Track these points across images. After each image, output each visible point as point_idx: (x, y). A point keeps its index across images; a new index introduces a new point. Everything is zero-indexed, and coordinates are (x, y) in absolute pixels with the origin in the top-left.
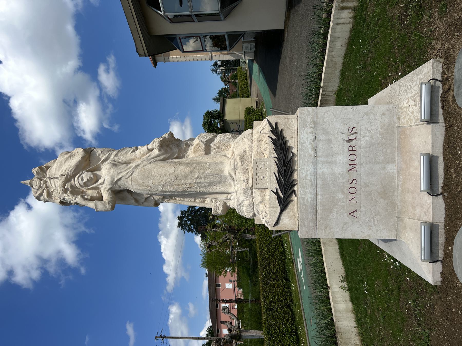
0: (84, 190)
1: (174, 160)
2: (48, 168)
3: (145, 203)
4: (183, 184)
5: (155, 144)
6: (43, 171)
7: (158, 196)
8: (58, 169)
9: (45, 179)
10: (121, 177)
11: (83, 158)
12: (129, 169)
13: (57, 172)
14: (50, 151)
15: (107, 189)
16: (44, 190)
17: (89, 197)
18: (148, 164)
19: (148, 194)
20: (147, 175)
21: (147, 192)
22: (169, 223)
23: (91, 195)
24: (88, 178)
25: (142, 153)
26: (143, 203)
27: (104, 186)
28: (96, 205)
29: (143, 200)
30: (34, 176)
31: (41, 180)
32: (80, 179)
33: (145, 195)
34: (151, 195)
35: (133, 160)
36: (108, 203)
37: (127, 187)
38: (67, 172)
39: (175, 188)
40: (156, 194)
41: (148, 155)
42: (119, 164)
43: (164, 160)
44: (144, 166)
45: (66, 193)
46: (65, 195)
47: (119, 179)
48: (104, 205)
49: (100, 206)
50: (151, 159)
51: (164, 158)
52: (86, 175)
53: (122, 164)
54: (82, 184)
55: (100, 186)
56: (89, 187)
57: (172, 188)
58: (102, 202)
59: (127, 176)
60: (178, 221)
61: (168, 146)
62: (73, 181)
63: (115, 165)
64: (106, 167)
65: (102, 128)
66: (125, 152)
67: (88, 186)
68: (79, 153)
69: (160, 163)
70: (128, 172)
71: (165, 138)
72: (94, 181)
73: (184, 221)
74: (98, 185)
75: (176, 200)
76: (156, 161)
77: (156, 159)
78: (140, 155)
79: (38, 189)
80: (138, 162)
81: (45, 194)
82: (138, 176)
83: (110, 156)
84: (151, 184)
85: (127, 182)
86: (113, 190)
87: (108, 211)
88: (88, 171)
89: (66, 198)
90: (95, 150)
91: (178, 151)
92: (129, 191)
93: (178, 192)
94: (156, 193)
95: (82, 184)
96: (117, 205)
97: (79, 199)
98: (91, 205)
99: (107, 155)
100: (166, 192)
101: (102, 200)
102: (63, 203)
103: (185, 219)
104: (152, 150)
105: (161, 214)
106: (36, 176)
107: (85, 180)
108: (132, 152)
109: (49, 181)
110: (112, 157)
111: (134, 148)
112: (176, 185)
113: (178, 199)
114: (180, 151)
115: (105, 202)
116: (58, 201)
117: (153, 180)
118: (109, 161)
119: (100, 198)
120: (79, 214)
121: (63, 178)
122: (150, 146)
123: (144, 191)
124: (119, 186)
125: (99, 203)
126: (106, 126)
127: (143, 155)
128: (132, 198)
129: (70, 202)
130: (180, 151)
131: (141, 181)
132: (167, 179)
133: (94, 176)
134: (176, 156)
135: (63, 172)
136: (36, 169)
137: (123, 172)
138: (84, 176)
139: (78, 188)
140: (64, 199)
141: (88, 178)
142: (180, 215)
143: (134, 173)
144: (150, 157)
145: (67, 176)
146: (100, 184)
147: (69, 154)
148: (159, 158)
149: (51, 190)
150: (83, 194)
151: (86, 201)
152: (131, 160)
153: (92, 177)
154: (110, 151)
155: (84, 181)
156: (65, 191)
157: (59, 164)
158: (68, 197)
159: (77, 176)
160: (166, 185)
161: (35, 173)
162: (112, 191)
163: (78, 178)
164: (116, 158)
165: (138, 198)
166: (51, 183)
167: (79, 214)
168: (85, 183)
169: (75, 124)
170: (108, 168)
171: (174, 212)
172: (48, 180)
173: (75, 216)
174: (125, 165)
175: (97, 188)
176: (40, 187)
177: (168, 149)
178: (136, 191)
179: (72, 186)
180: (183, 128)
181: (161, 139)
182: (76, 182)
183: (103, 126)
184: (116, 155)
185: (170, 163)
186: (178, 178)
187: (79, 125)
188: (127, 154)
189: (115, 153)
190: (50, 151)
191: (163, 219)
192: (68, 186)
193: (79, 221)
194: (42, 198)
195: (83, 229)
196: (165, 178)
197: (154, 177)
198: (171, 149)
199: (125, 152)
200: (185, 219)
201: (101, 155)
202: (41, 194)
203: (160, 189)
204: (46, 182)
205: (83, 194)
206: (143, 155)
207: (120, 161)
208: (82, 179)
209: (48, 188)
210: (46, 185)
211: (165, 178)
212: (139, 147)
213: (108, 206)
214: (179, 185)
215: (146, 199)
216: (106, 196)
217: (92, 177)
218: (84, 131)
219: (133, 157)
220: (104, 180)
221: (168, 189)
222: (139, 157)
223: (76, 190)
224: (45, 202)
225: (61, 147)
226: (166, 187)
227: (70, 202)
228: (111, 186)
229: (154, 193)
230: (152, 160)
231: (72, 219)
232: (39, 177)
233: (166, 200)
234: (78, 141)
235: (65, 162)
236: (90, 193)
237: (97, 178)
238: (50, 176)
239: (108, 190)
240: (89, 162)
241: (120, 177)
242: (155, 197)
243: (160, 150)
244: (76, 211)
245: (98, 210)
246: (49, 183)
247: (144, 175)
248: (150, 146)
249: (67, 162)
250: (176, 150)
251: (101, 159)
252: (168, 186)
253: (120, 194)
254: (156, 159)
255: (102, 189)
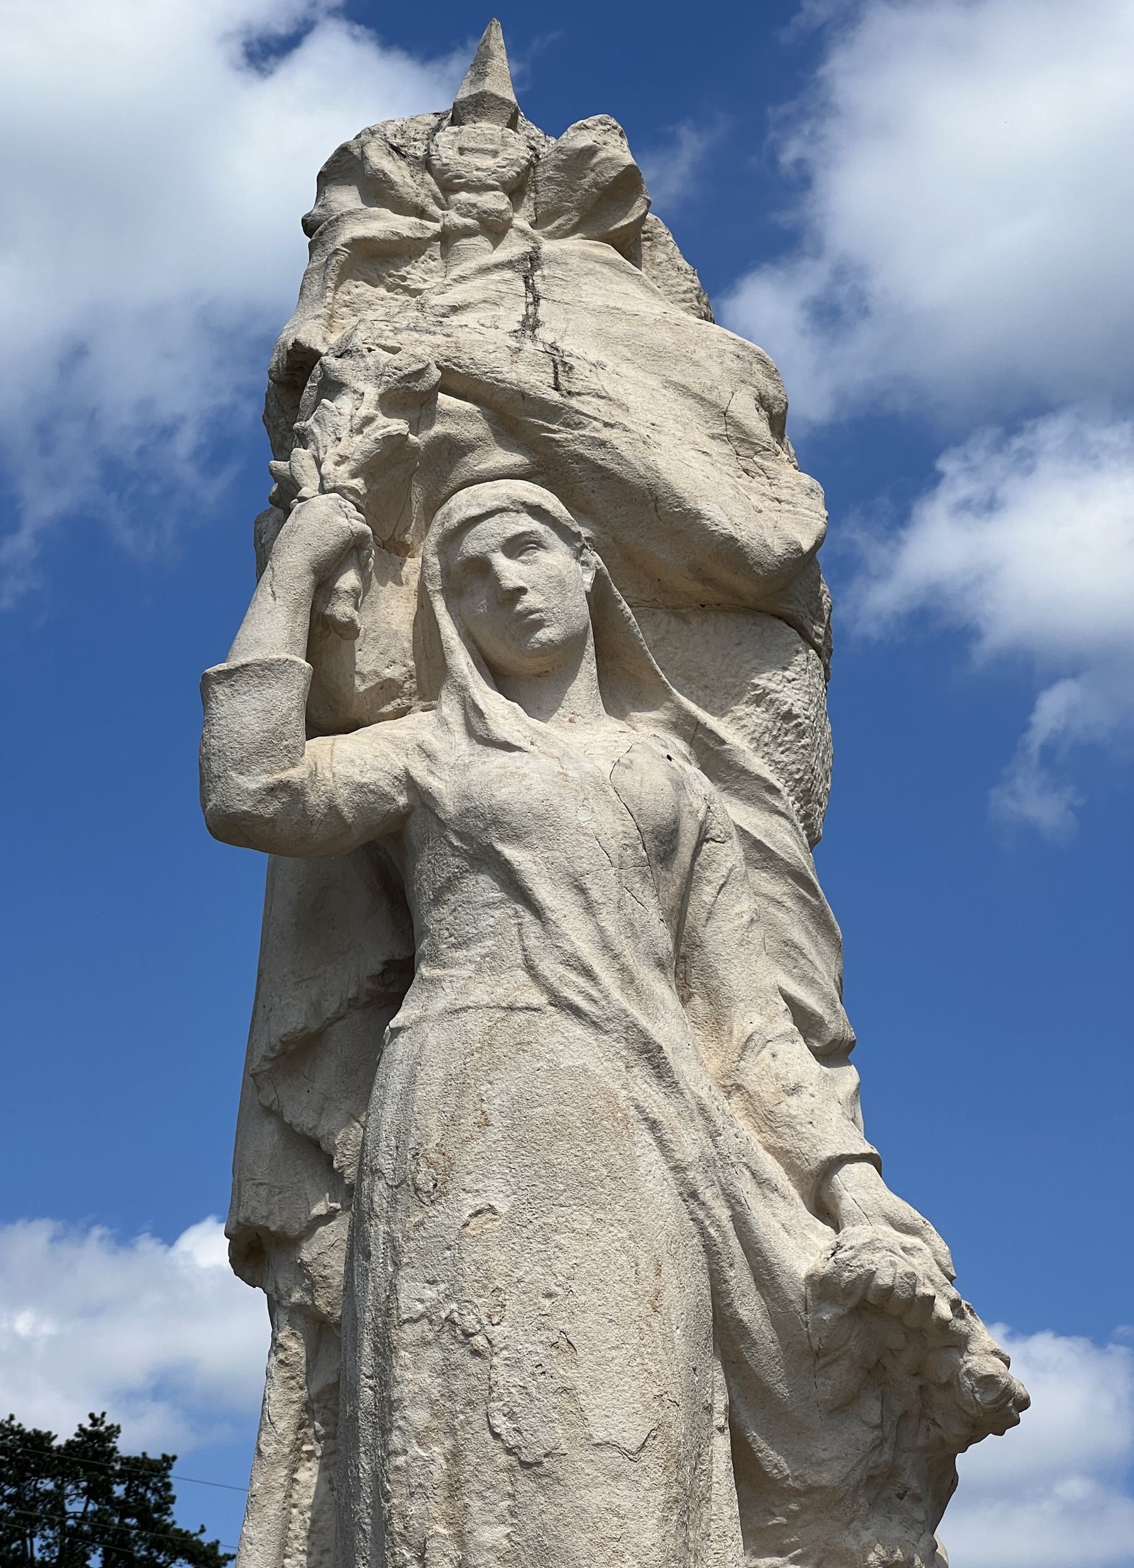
0: (411, 567)
1: (722, 1445)
2: (629, 245)
3: (267, 1136)
4: (461, 1538)
5: (890, 1239)
6: (602, 209)
7: (335, 1265)
8: (619, 328)
9: (521, 221)
10: (537, 911)
11: (730, 550)
12: (628, 978)
13: (591, 322)
14: (784, 218)
15: (420, 771)
16: (421, 212)
17: (342, 609)
18: (678, 1168)
19: (367, 1168)
20: (564, 1156)
21: (385, 1163)
22: (47, 1328)
23: (363, 621)
24: (530, 600)
25: (793, 1105)
26: (272, 1112)
27: (456, 744)
28: (267, 669)
29: (300, 1115)
30: (554, 129)
31: (516, 190)
32: (526, 523)
33: (355, 1133)
34: (350, 1195)
35: (717, 1022)
36: (285, 786)
37: (435, 959)
38: (587, 405)
39: (419, 1456)
40: (358, 1246)
41: (772, 1168)
42: (675, 880)
43: (725, 1335)
44: (654, 1126)
45: (390, 403)
46: (372, 392)
47: (515, 888)
48: (270, 747)
49: (253, 713)
50: (732, 1201)
51: (742, 1330)
52: (561, 584)
53: (678, 918)
54: (472, 545)
55: (450, 708)
56: (439, 605)
57: (419, 1416)
58: (298, 723)
59: (549, 967)
60: (64, 1433)
61: (874, 1373)
62: (503, 458)
63: (665, 848)
64: (640, 759)
65: (1024, 674)
66: (798, 935)
67: (454, 592)
68: (773, 511)
69: (683, 1291)
70: (587, 973)
71: (961, 1343)
72: (501, 652)
73: (56, 1499)
74: (462, 689)
75: (297, 1457)
76: (710, 1250)
77: (729, 1250)
78: (766, 1090)
79: (426, 164)
80: (696, 1070)
81: (384, 223)
82: (554, 1070)
83: (751, 799)
84: (472, 1202)
85: (492, 964)
86: (416, 827)
87: (205, 781)
88: (599, 598)
89: (344, 403)
90: (805, 661)
91: (825, 1478)
92: (396, 979)
93: (378, 1478)
94: (378, 1250)
95: (472, 545)
96: (259, 860)
97: (324, 518)
98: (271, 629)
99: (758, 765)
100: (385, 1350)
101: (315, 728)
102: (298, 377)
103: (76, 1506)
104: (825, 1209)
105: (147, 1245)
106: (548, 147)
107: (511, 572)
108: (796, 1008)
109: (502, 254)
110: (738, 813)
111: (838, 1024)
112: (455, 1456)
113: (309, 1474)
114: (822, 1501)
115: (293, 755)
116: (311, 333)
117: (515, 1224)
118: (701, 784)
119: (331, 710)
120: (188, 473)
121: (532, 376)
122: (859, 1186)
123: (402, 1133)
124: (450, 885)
125: (286, 698)
126: (1053, 708)
127: (767, 1120)
128: (331, 1006)
129: (303, 439)
130: (822, 1501)
131: (498, 1093)
132: (515, 1364)
133: (550, 647)
134: (772, 1458)
135: (583, 377)
136: (618, 151)
137: (597, 926)
138: (557, 558)
139: (432, 507)
140: (333, 387)
141: (530, 600)
142: (127, 1445)
143: (577, 1030)
144: (745, 1186)
145: (553, 412)
146: (473, 713)
147: (759, 426)
148: (739, 1277)
149: (415, 274)
150: (372, 550)
151: (305, 584)
152: (713, 996)
153: (544, 635)
154: (806, 797)
155: (501, 563)
156: (408, 396)
157: (664, 337)
158: (346, 428)
159: (551, 502)
160: (459, 1354)
161: (578, 138)
162: (403, 817)
163: (537, 512)
164: (728, 856)
165: (326, 1072)
166: (485, 270)
167: (188, 473)
168: (482, 567)
169: (1051, 433)
170: (627, 779)
171: (165, 1387)
172: (513, 248)
173: (167, 432)
174: (665, 942)
175: (430, 677)
176: (449, 184)
177: (838, 1378)
178: (399, 1050)
179: (452, 450)
180: (1075, 1488)
181: (943, 1309)
182: (496, 496)
183: (1052, 679)
184: (760, 854)
185: (693, 1392)
186: (526, 1485)
187: (1046, 467)
188: (768, 954)
189: (786, 840)
190: (784, 218)
191: (94, 1265)
192: (457, 417)
193: (114, 474)
194: (346, 198)
195: (43, 505)
196: (533, 1347)
197: (546, 1234)
198: (842, 1407)
199: (798, 935)
200: (76, 1506)
201: (758, 717)
202: (378, 191)
203: (414, 1295)
204: (494, 228)
205: (372, 550)
206: (767, 1120)
207: (706, 893)
208: (516, 546)
209: (436, 250)
210: (468, 232)
211: (533, 1347)
212: (848, 1077)
213: (255, 781)
214: (454, 1488)
215: (314, 1151)
216: (353, 763)
217: (544, 635)
218: (990, 506)
219: (747, 1020)
220: (508, 747)
221: (416, 1376)
222: (750, 1081)
223: (417, 494)
224: (309, 226)
225: (829, 316)
226: (434, 1355)
227: (303, 439)
228: (450, 806)
229: (378, 1229)
230: (723, 1213)
231: (145, 404)
232: (545, 172)
233: (296, 1347)
234: (880, 456)
235: (684, 390)
236: (386, 619)
237: (533, 677)
238: (555, 261)
239: (410, 783)
240: (679, 602)
241: (544, 891)
242: (336, 1233)
243: (823, 1287)
244: (217, 450)
245: (220, 691)
246: (479, 252)
247: (559, 1130)
248: (859, 1186)
249: (684, 407)
250: (834, 1456)
251: (720, 711)
252: (447, 1370)
253: (371, 894)
254: (729, 1250)
255: (418, 725)
